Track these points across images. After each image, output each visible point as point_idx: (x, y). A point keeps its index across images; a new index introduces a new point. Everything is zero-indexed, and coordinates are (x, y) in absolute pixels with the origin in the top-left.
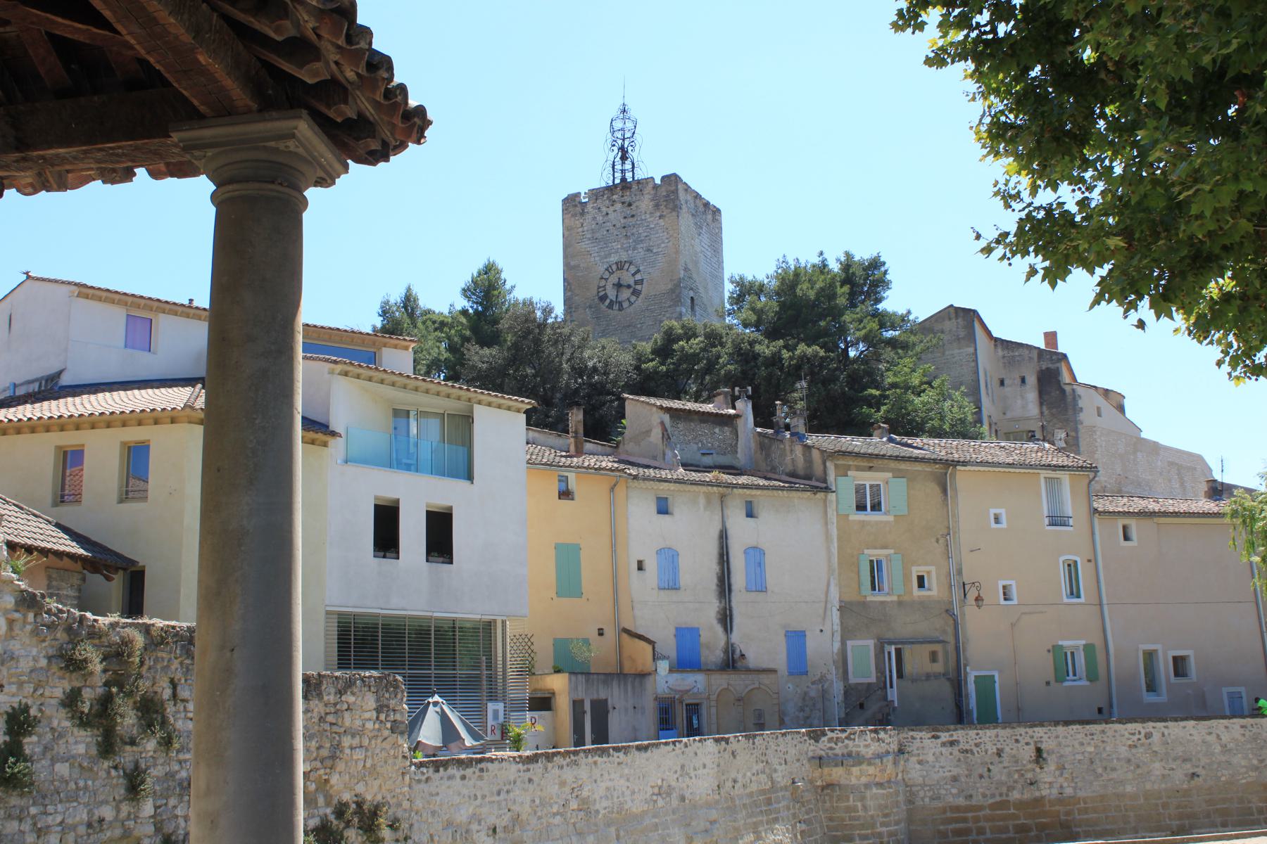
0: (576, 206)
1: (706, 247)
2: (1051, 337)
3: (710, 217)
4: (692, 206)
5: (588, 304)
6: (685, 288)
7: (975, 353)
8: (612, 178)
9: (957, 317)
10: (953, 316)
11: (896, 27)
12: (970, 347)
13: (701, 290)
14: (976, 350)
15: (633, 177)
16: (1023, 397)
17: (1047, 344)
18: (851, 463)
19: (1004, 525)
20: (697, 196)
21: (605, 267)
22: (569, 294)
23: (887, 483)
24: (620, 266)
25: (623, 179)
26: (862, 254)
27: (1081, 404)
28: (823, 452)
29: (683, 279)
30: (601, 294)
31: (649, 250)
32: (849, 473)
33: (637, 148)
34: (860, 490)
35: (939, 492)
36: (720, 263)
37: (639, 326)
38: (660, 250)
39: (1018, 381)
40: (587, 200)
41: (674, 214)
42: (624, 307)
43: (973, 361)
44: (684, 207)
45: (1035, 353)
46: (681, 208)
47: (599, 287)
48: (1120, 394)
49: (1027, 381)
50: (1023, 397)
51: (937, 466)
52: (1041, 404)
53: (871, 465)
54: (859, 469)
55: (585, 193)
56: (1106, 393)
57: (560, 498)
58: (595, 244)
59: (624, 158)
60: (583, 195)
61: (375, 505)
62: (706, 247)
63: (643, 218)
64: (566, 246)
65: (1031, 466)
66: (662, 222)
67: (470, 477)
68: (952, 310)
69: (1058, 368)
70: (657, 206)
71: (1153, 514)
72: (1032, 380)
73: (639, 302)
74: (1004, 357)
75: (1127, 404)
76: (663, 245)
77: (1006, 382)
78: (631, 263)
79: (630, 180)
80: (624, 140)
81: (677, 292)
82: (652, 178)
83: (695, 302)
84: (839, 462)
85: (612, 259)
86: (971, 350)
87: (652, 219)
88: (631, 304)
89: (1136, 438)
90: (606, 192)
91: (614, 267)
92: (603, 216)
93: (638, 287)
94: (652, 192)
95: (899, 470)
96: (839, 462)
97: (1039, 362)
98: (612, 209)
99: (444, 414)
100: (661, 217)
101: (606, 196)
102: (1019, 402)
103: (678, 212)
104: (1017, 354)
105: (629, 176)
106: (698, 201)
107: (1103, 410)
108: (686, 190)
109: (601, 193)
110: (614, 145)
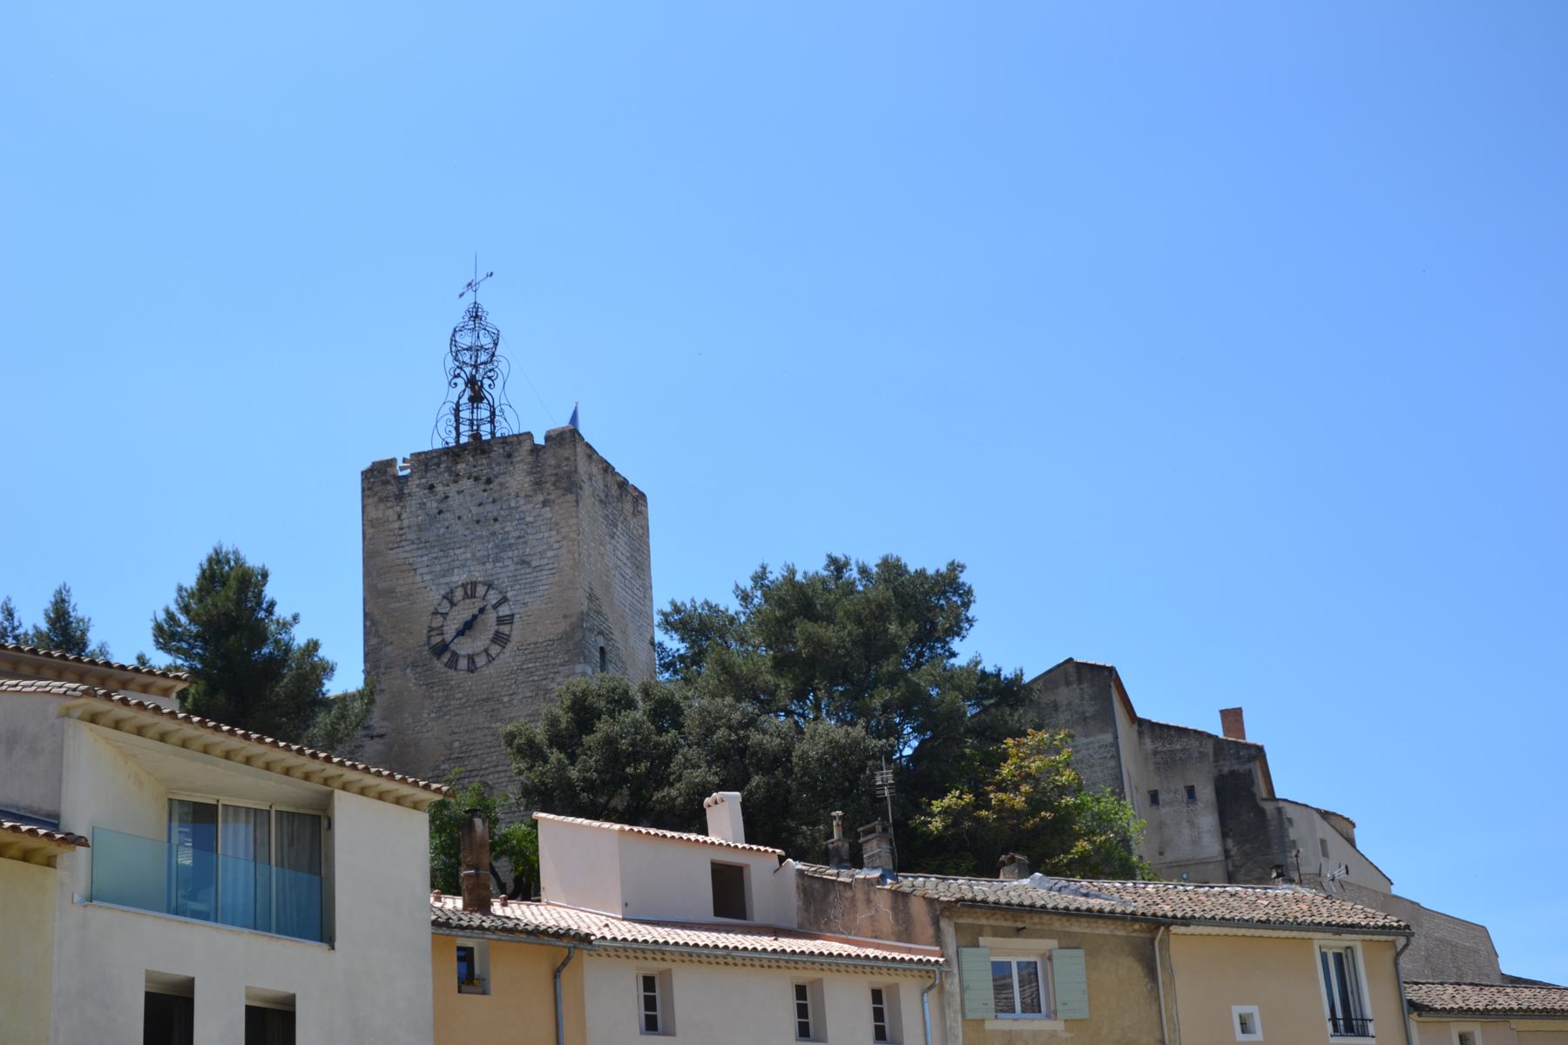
0: (387, 483)
1: (624, 558)
2: (1232, 718)
3: (628, 507)
4: (601, 485)
5: (409, 660)
6: (591, 630)
7: (1115, 744)
8: (454, 434)
9: (1080, 681)
10: (1073, 678)
11: (179, 584)
12: (1105, 732)
13: (617, 636)
14: (1116, 738)
15: (493, 433)
16: (1192, 824)
17: (1226, 730)
18: (983, 921)
19: (1258, 1036)
20: (607, 468)
21: (443, 592)
22: (374, 641)
23: (1050, 959)
24: (470, 589)
25: (476, 436)
26: (924, 558)
27: (1293, 834)
28: (931, 902)
29: (588, 614)
30: (436, 640)
31: (524, 562)
32: (982, 941)
33: (499, 382)
34: (1000, 973)
35: (1142, 974)
36: (647, 588)
37: (506, 699)
38: (546, 561)
39: (1183, 795)
40: (407, 472)
41: (570, 497)
42: (478, 665)
43: (1112, 757)
44: (586, 486)
45: (1209, 748)
46: (581, 488)
47: (431, 629)
48: (1348, 819)
49: (1197, 794)
50: (1192, 824)
51: (1137, 927)
52: (1224, 835)
53: (1020, 925)
54: (997, 932)
55: (404, 460)
56: (1326, 815)
57: (460, 991)
58: (424, 551)
59: (477, 398)
60: (400, 464)
61: (148, 995)
62: (624, 558)
63: (513, 505)
64: (369, 556)
65: (1299, 926)
66: (547, 513)
67: (324, 933)
68: (1071, 669)
69: (1250, 770)
70: (538, 484)
71: (1508, 1013)
72: (1206, 793)
73: (508, 657)
74: (1155, 753)
75: (1359, 835)
76: (550, 554)
77: (1162, 797)
78: (490, 586)
79: (486, 437)
80: (476, 366)
81: (578, 636)
82: (529, 435)
83: (608, 657)
84: (962, 921)
85: (455, 578)
86: (1108, 738)
87: (530, 506)
88: (472, 668)
89: (1385, 895)
90: (444, 458)
91: (459, 594)
92: (438, 501)
93: (505, 629)
94: (530, 459)
95: (1069, 935)
96: (962, 921)
97: (1216, 761)
98: (454, 488)
99: (269, 812)
100: (545, 503)
101: (443, 466)
102: (1186, 831)
103: (577, 495)
104: (1178, 747)
105: (485, 430)
106: (609, 478)
107: (1329, 845)
108: (590, 457)
109: (436, 460)
110: (458, 376)
